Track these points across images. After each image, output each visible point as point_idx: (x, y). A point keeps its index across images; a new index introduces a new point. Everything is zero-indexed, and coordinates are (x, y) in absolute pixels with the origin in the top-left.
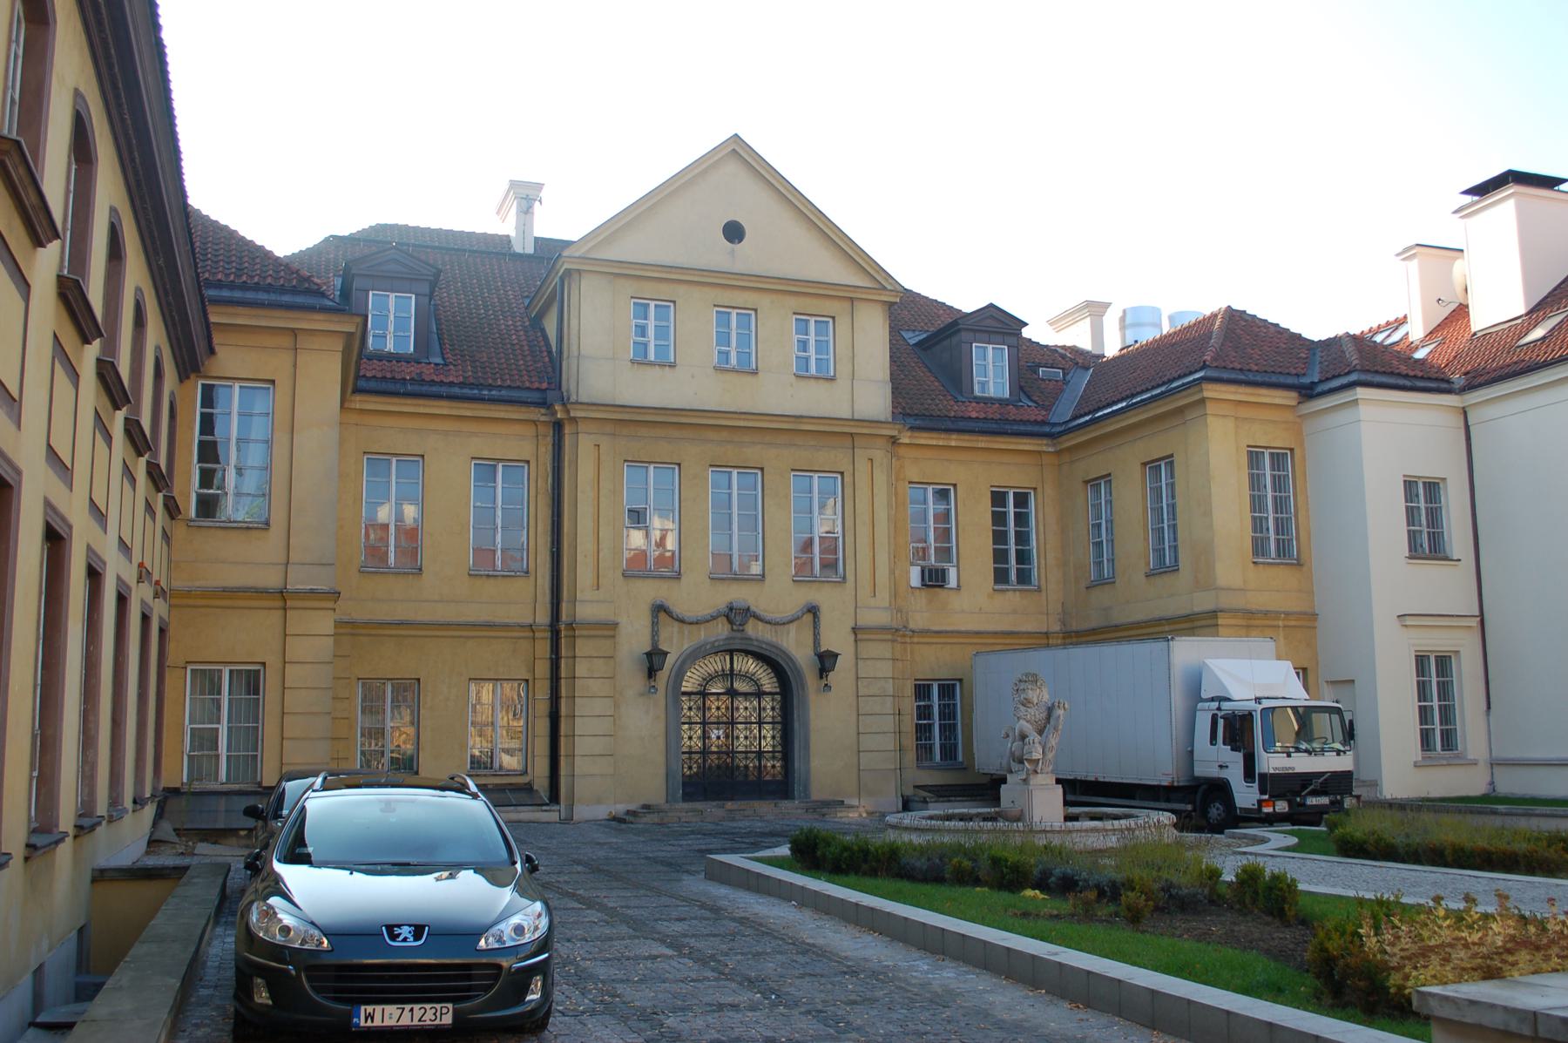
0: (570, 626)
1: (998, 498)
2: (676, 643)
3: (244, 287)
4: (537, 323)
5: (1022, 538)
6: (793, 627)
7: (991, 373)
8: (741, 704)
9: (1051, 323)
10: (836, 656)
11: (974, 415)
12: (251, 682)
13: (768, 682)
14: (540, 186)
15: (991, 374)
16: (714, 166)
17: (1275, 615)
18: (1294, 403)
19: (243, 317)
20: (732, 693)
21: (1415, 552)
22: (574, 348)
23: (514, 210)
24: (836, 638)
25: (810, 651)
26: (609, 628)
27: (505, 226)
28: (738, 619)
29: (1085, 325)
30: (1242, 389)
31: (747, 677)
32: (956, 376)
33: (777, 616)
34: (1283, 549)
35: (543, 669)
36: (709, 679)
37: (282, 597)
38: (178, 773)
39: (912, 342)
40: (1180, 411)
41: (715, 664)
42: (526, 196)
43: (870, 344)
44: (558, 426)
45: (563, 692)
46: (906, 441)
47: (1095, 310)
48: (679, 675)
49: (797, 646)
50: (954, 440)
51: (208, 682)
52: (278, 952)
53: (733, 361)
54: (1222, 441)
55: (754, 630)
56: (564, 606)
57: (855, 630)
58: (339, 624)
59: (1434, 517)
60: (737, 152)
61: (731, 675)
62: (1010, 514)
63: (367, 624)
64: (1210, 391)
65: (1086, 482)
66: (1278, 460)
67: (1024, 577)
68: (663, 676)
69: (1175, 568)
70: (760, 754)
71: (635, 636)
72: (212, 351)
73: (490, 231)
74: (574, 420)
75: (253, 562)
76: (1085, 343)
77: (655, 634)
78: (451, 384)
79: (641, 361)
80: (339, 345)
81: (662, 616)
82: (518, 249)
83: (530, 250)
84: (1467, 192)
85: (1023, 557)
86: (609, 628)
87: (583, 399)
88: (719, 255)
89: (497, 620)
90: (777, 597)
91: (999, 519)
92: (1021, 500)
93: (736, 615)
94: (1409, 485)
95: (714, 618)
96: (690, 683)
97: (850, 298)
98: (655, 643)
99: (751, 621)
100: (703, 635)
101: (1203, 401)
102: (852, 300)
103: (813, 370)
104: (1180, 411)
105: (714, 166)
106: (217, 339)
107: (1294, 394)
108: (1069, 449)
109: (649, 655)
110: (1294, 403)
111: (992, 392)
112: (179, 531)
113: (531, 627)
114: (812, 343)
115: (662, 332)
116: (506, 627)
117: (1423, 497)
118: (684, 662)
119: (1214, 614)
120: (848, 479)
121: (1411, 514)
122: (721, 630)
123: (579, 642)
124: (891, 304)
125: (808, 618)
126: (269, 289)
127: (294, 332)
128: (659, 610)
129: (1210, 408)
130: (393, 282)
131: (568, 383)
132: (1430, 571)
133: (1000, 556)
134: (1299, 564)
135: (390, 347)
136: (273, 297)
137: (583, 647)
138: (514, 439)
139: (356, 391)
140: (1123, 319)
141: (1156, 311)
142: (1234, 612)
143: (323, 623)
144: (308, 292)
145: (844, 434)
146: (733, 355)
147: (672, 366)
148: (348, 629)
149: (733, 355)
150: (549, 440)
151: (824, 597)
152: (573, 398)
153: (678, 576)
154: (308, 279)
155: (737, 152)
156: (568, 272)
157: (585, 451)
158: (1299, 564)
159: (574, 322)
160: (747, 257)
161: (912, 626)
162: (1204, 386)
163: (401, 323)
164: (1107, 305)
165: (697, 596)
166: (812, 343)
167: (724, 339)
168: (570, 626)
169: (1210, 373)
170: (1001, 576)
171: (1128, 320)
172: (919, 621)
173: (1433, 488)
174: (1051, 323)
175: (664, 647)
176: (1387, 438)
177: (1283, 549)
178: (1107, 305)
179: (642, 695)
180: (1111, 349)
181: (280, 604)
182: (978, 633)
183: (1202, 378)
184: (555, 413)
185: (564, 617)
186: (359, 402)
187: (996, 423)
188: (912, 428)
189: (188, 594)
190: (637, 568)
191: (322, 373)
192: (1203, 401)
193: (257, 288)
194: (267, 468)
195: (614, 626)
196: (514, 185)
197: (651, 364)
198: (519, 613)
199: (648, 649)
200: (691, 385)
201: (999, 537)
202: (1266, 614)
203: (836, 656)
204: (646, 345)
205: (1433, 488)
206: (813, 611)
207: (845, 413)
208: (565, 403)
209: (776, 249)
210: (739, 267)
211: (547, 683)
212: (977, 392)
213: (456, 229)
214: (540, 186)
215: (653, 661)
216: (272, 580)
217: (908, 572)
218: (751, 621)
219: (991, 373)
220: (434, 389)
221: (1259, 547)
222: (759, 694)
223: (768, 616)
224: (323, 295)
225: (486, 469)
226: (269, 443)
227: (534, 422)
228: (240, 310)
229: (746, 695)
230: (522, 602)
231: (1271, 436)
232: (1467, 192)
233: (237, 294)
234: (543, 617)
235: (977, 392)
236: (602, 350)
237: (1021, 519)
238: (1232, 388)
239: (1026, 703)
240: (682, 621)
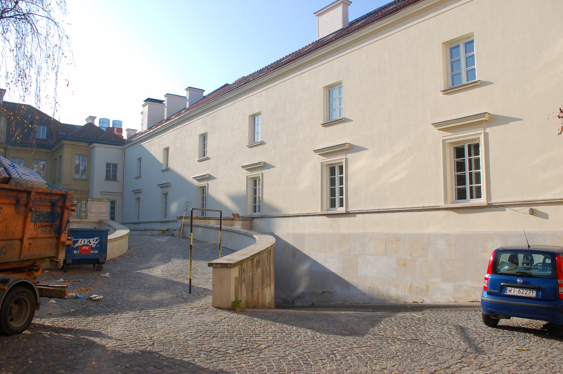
21: (108, 178)
59: (115, 172)
94: (108, 165)
121: (108, 171)
141: (108, 121)
164: (96, 117)
173: (115, 166)
176: (103, 154)
178: (96, 117)
192: (63, 144)
205: (115, 166)
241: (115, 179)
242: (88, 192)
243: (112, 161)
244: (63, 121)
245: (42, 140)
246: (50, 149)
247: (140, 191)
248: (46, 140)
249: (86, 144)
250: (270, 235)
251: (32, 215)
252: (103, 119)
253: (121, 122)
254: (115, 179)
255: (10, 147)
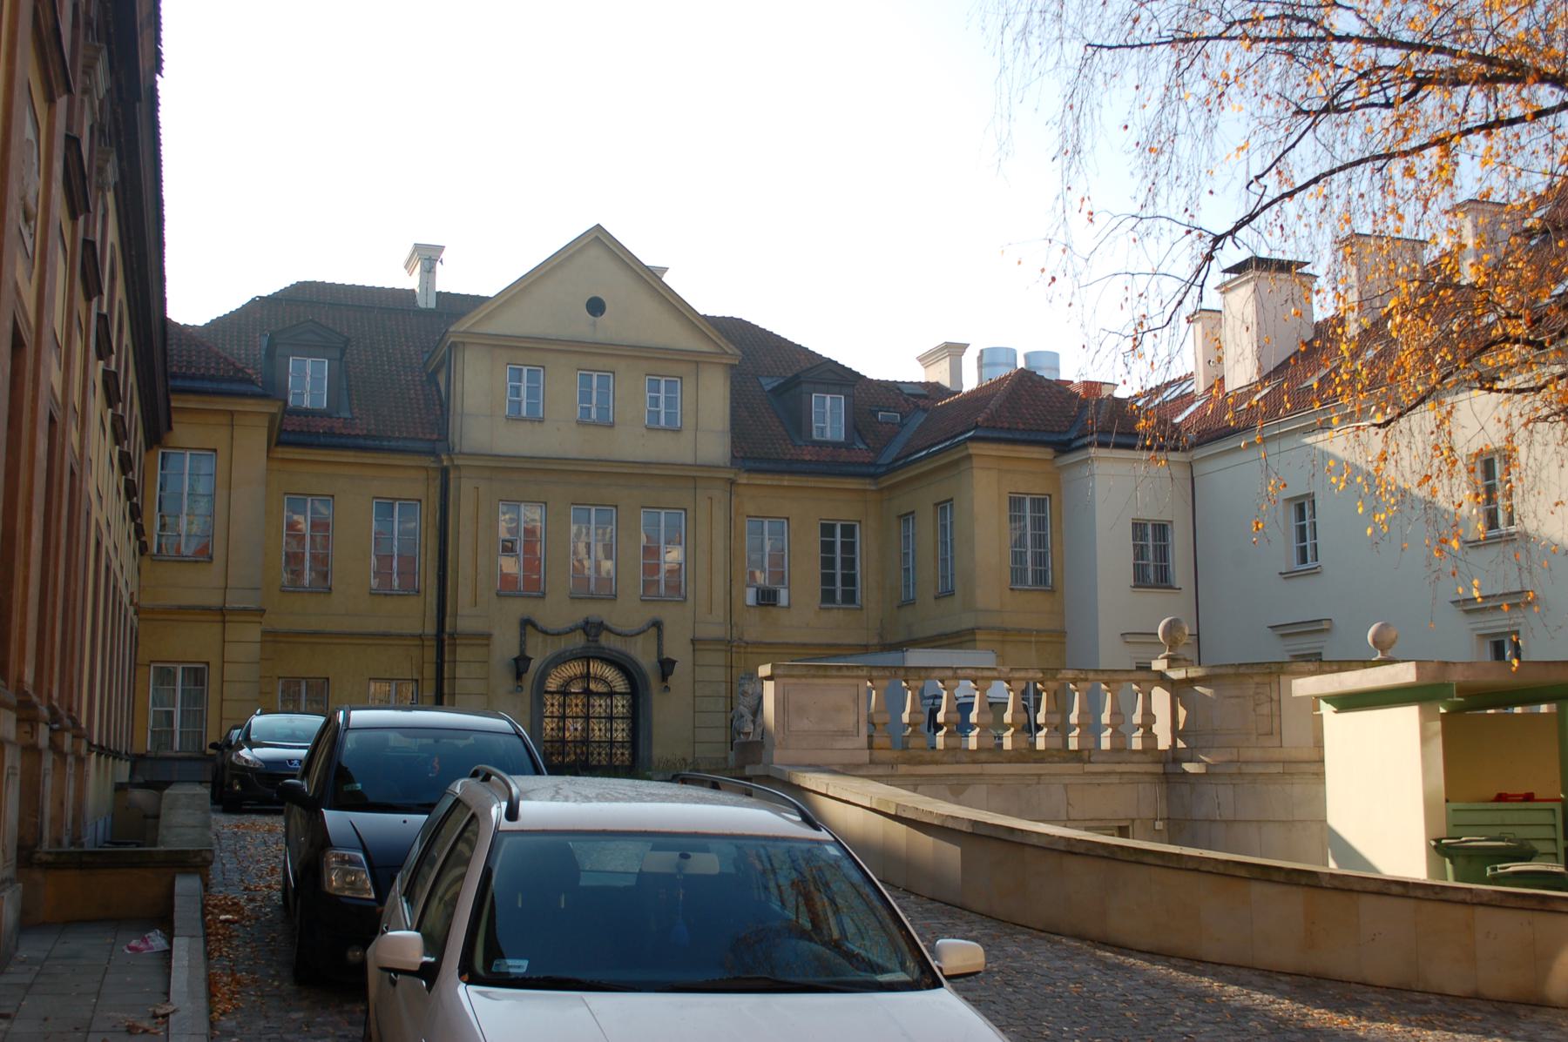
0: (452, 636)
1: (827, 530)
2: (539, 652)
3: (193, 378)
4: (432, 377)
5: (849, 563)
6: (640, 639)
7: (828, 418)
8: (597, 701)
9: (921, 359)
10: (674, 662)
11: (808, 457)
12: (197, 676)
13: (620, 684)
14: (443, 248)
15: (828, 420)
16: (580, 251)
17: (1029, 632)
18: (1050, 457)
19: (193, 403)
20: (588, 692)
21: (1140, 580)
22: (459, 409)
23: (418, 269)
24: (676, 648)
25: (655, 660)
26: (485, 638)
27: (411, 282)
28: (593, 631)
29: (945, 365)
30: (1002, 447)
31: (601, 679)
32: (798, 421)
33: (626, 629)
34: (1040, 577)
35: (430, 671)
36: (569, 681)
37: (222, 613)
38: (146, 744)
39: (768, 388)
40: (956, 463)
41: (574, 669)
42: (427, 257)
43: (712, 400)
44: (445, 472)
45: (446, 690)
46: (744, 481)
47: (954, 351)
48: (543, 676)
49: (643, 654)
50: (786, 481)
51: (165, 676)
52: (243, 768)
53: (594, 416)
54: (987, 489)
55: (606, 640)
56: (448, 620)
57: (693, 641)
58: (265, 633)
59: (1162, 553)
60: (598, 238)
61: (587, 676)
62: (837, 548)
63: (287, 634)
64: (974, 449)
65: (900, 517)
66: (1039, 504)
67: (849, 597)
68: (529, 678)
69: (952, 593)
70: (612, 743)
71: (506, 644)
72: (170, 428)
73: (399, 286)
74: (457, 467)
75: (198, 587)
76: (946, 381)
77: (523, 644)
78: (357, 436)
79: (515, 418)
80: (265, 422)
81: (529, 628)
82: (421, 304)
83: (432, 305)
84: (1225, 271)
85: (849, 580)
86: (485, 638)
87: (466, 449)
88: (581, 326)
89: (393, 631)
90: (626, 614)
91: (828, 547)
92: (848, 531)
93: (592, 628)
94: (1138, 527)
95: (572, 630)
96: (553, 684)
97: (696, 361)
98: (522, 651)
99: (604, 633)
100: (564, 644)
101: (969, 457)
102: (697, 363)
103: (663, 422)
104: (956, 463)
105: (580, 251)
106: (175, 417)
107: (1050, 450)
108: (892, 488)
109: (516, 660)
110: (1050, 457)
111: (828, 436)
112: (146, 562)
113: (420, 637)
114: (662, 399)
115: (533, 393)
116: (401, 636)
117: (1151, 540)
118: (547, 667)
119: (972, 631)
120: (690, 514)
121: (1140, 552)
122: (579, 640)
123: (459, 650)
124: (732, 366)
125: (653, 631)
126: (212, 379)
127: (232, 413)
128: (527, 624)
129: (976, 462)
130: (309, 349)
131: (454, 437)
132: (1153, 598)
133: (828, 579)
134: (1053, 591)
135: (307, 403)
136: (215, 385)
137: (462, 653)
138: (409, 482)
139: (280, 443)
140: (980, 358)
141: (1013, 353)
142: (990, 629)
143: (253, 632)
144: (241, 381)
145: (688, 477)
146: (594, 411)
147: (541, 421)
148: (272, 637)
149: (594, 411)
150: (438, 482)
151: (667, 614)
152: (457, 449)
153: (543, 596)
154: (241, 370)
155: (598, 238)
156: (454, 344)
157: (466, 491)
158: (1053, 591)
159: (459, 385)
160: (609, 327)
161: (746, 638)
162: (969, 444)
163: (316, 382)
164: (966, 346)
165: (558, 612)
166: (662, 399)
167: (586, 397)
168: (452, 636)
169: (981, 433)
170: (828, 596)
171: (985, 360)
172: (751, 634)
173: (1161, 529)
174: (921, 359)
175: (529, 654)
176: (1117, 489)
177: (1040, 577)
178: (966, 346)
179: (511, 693)
180: (970, 382)
181: (219, 618)
182: (804, 645)
183: (971, 439)
184: (441, 461)
185: (447, 629)
186: (282, 452)
187: (829, 464)
188: (749, 471)
189: (152, 610)
190: (507, 589)
191: (253, 440)
192: (969, 457)
193: (203, 378)
194: (212, 515)
195: (488, 636)
196: (418, 248)
197: (523, 420)
198: (412, 625)
199: (516, 654)
200: (556, 438)
201: (828, 563)
202: (1019, 631)
203: (674, 662)
204: (520, 403)
205: (1161, 529)
206: (657, 625)
207: (689, 460)
208: (449, 451)
209: (630, 321)
210: (600, 337)
211: (433, 683)
212: (815, 436)
213: (368, 284)
214: (443, 248)
215: (520, 665)
216: (214, 600)
217: (744, 593)
218: (604, 633)
219: (828, 418)
220: (343, 441)
221: (1017, 575)
222: (611, 694)
223: (619, 629)
224: (253, 382)
225: (386, 508)
226: (212, 497)
227: (426, 469)
228: (191, 397)
229: (600, 695)
230: (415, 616)
231: (1038, 487)
232: (1225, 271)
233: (188, 384)
234: (431, 629)
235: (815, 436)
236: (483, 406)
237: (849, 547)
238: (994, 446)
239: (744, 693)
240: (545, 632)
241: (1163, 580)
242: (1063, 633)
243: (1151, 513)
244: (201, 323)
245: (308, 413)
246: (874, 476)
247: (1325, 625)
248: (847, 445)
249: (1046, 453)
250: (824, 771)
251: (1149, 735)
252: (993, 350)
253: (1056, 356)
254: (1163, 580)
255: (743, 479)
